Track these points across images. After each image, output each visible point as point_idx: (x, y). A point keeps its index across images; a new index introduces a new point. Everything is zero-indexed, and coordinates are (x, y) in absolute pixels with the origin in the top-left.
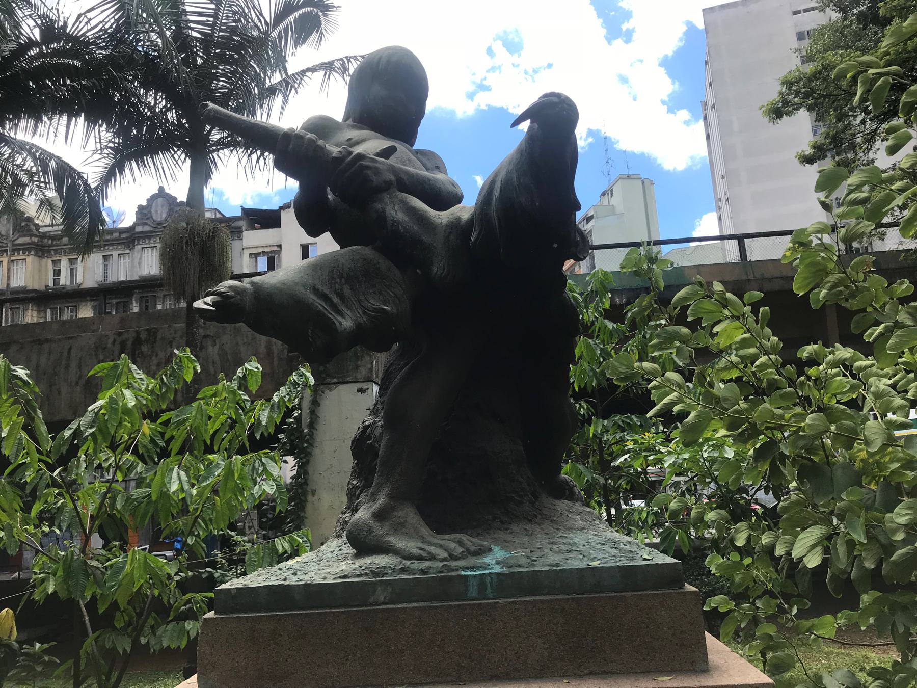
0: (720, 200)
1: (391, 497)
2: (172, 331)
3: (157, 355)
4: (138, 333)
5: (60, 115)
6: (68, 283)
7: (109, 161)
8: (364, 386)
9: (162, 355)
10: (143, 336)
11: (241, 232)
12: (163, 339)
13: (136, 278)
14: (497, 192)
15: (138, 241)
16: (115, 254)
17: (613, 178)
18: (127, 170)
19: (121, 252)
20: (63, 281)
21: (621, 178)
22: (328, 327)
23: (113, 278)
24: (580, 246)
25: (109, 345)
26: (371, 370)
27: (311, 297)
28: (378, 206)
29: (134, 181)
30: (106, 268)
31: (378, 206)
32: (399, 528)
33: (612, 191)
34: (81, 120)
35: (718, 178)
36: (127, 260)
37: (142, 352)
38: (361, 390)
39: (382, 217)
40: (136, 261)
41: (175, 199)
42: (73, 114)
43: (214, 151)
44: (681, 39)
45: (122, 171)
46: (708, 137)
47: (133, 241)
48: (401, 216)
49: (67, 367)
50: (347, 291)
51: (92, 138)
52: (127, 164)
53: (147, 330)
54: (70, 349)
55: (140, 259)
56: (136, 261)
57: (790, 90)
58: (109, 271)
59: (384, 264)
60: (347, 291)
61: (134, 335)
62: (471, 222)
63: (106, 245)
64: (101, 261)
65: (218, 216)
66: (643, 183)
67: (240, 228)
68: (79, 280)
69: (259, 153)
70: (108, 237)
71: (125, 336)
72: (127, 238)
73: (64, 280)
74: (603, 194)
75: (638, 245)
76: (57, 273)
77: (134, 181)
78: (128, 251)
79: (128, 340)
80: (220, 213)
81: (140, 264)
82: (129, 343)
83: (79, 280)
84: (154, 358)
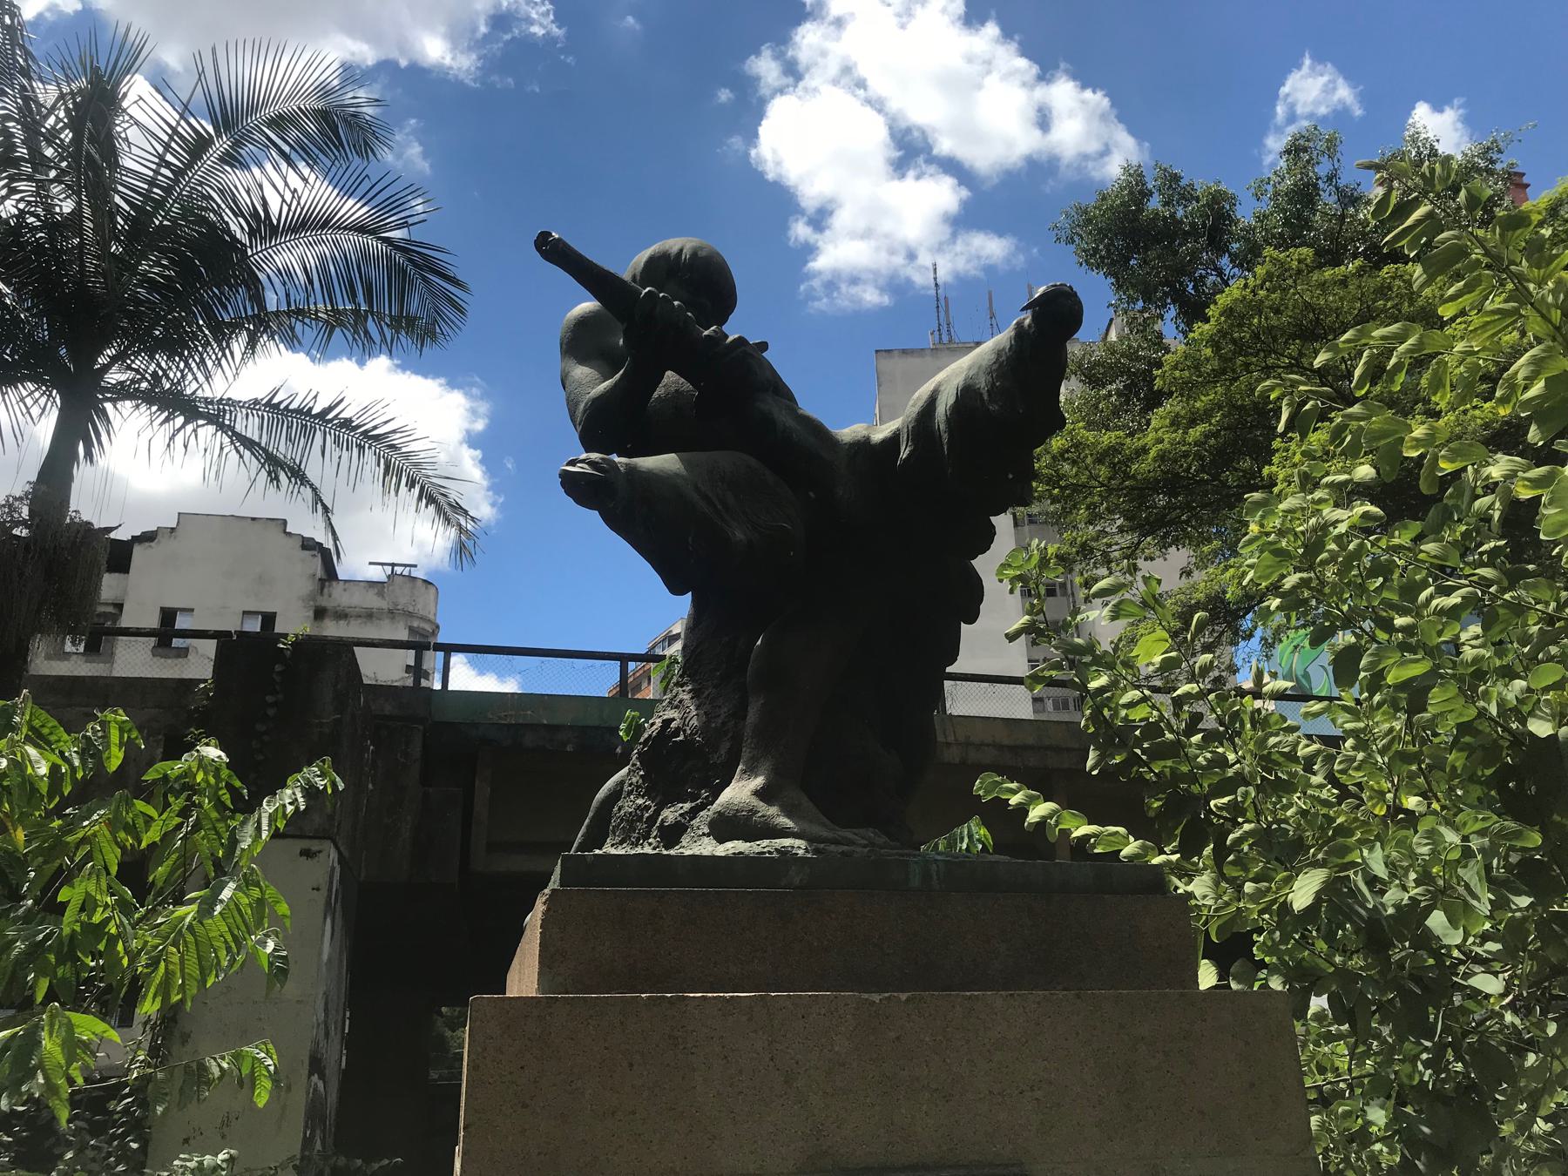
8: (314, 845)
14: (941, 410)
38: (307, 853)
48: (791, 422)
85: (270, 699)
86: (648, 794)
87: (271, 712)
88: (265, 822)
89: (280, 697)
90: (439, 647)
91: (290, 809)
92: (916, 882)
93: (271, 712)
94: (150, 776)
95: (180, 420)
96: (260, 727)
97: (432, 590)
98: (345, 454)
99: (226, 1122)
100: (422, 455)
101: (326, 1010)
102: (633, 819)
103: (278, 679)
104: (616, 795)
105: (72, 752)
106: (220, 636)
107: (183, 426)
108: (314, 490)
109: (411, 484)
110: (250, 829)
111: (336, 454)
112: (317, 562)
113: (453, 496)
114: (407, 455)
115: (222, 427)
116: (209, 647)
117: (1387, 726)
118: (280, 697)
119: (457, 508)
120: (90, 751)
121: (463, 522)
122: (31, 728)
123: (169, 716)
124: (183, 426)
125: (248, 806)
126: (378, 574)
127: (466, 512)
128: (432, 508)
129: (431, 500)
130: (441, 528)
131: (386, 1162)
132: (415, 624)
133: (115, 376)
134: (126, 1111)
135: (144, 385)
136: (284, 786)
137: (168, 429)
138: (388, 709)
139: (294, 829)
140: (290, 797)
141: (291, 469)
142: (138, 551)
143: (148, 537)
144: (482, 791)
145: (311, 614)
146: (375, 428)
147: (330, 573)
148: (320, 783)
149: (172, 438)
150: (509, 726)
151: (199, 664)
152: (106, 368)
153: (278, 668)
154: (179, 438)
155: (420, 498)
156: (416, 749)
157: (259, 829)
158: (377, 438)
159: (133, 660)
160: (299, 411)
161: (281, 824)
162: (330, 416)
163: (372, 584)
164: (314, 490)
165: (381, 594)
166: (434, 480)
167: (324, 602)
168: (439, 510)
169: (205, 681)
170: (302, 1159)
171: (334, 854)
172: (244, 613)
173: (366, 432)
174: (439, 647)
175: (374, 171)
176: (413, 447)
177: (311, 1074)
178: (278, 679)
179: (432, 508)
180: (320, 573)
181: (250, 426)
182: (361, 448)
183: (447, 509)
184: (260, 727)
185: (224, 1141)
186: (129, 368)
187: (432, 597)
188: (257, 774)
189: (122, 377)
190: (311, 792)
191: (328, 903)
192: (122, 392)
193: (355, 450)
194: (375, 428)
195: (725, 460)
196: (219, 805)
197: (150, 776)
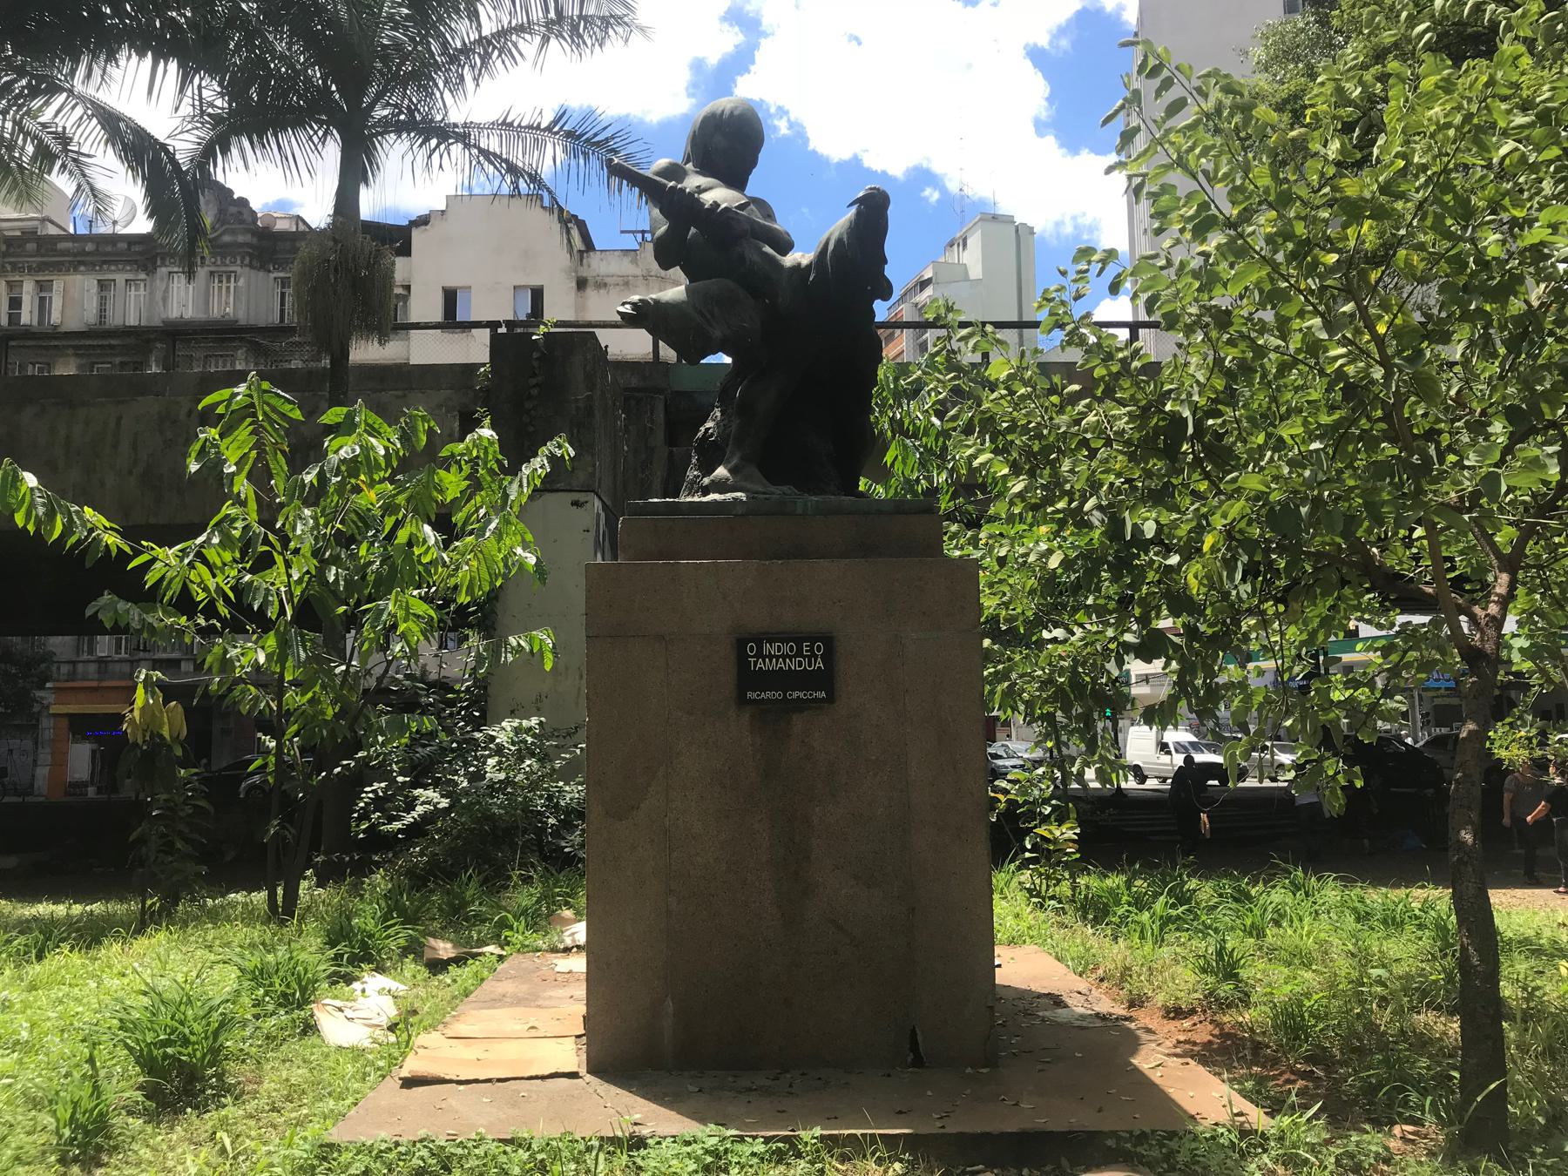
1: (742, 459)
5: (142, 55)
6: (35, 323)
7: (205, 134)
8: (581, 497)
13: (157, 322)
14: (831, 247)
15: (163, 259)
16: (120, 278)
18: (235, 151)
19: (130, 276)
20: (25, 319)
23: (114, 320)
24: (885, 291)
25: (182, 417)
26: (592, 475)
29: (247, 167)
30: (103, 302)
34: (173, 66)
35: (1138, 232)
36: (142, 292)
38: (576, 504)
40: (159, 295)
41: (230, 192)
42: (161, 55)
43: (376, 135)
44: (1061, 31)
45: (225, 151)
47: (153, 260)
48: (756, 258)
49: (115, 446)
51: (187, 100)
52: (234, 139)
54: (120, 419)
55: (166, 290)
56: (159, 295)
58: (109, 307)
62: (809, 266)
63: (105, 262)
64: (95, 289)
65: (302, 227)
68: (55, 317)
70: (109, 249)
72: (140, 253)
73: (27, 316)
76: (15, 303)
77: (247, 167)
78: (143, 276)
80: (305, 222)
81: (165, 300)
83: (55, 317)
85: (533, 381)
86: (699, 469)
87: (535, 392)
92: (799, 511)
93: (535, 392)
94: (444, 453)
95: (434, 142)
96: (528, 405)
99: (539, 699)
100: (639, 156)
102: (693, 482)
103: (536, 364)
105: (394, 438)
106: (493, 325)
107: (438, 146)
108: (550, 192)
110: (515, 486)
115: (467, 146)
116: (484, 335)
120: (405, 438)
122: (367, 424)
123: (460, 396)
124: (438, 146)
125: (514, 470)
133: (380, 112)
134: (468, 688)
135: (402, 117)
136: (535, 455)
137: (424, 151)
138: (634, 382)
139: (549, 485)
140: (538, 466)
141: (530, 175)
142: (417, 235)
143: (423, 221)
145: (574, 284)
146: (596, 135)
148: (558, 453)
149: (430, 157)
151: (475, 349)
152: (371, 106)
153: (535, 355)
154: (436, 156)
156: (660, 416)
157: (521, 486)
158: (598, 144)
159: (428, 349)
160: (530, 127)
161: (538, 482)
164: (550, 192)
165: (634, 262)
167: (584, 272)
169: (484, 365)
171: (597, 503)
173: (588, 140)
175: (311, 925)
178: (536, 364)
181: (492, 143)
182: (585, 154)
185: (538, 712)
186: (388, 104)
188: (517, 450)
189: (385, 112)
190: (552, 459)
191: (597, 542)
192: (389, 126)
194: (596, 135)
196: (491, 472)
197: (444, 453)
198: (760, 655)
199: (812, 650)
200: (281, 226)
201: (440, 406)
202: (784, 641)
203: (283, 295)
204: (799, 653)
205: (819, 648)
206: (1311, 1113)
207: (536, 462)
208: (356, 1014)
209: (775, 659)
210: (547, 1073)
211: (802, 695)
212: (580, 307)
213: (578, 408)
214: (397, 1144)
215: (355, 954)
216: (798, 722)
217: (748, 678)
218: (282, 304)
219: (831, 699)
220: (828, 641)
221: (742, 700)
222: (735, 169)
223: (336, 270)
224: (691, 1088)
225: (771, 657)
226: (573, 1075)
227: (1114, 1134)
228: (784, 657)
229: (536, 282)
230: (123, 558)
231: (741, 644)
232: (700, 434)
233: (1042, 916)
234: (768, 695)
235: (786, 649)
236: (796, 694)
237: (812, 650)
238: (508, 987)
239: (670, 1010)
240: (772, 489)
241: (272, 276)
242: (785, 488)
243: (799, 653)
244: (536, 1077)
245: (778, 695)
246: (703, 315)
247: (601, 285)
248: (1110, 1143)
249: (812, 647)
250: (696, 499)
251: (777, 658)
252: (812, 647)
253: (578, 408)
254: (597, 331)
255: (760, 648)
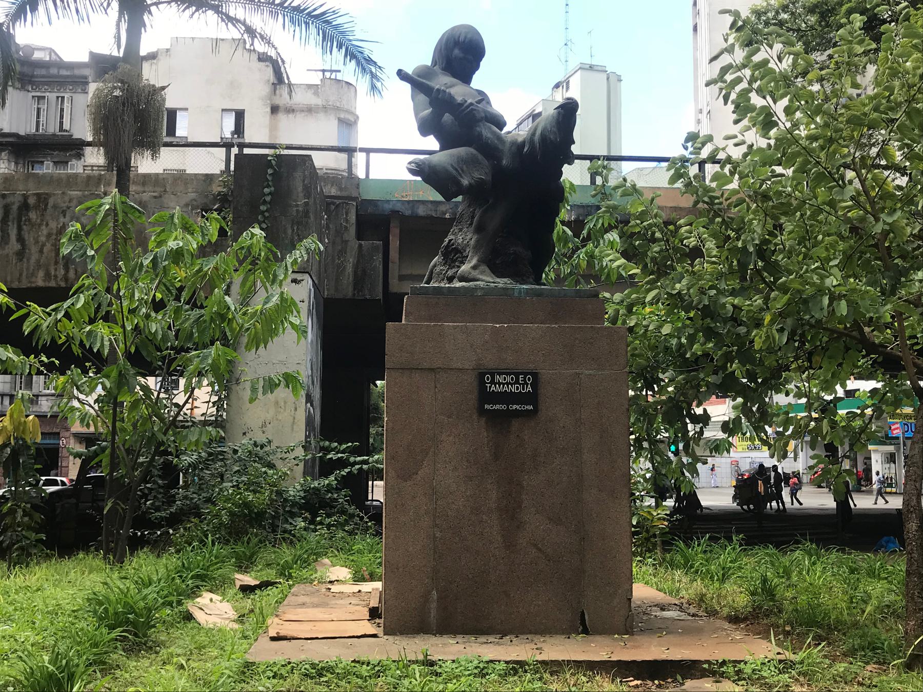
0: (701, 111)
1: (478, 261)
2: (67, 198)
3: (47, 225)
4: (25, 197)
8: (299, 277)
9: (53, 225)
10: (32, 201)
11: (87, 83)
12: (55, 207)
14: (538, 132)
17: (573, 64)
18: (41, 8)
21: (582, 68)
22: (458, 183)
27: (451, 169)
28: (478, 129)
29: (50, 23)
31: (478, 129)
32: (482, 273)
33: (568, 83)
37: (29, 220)
39: (480, 135)
45: (34, 9)
46: (695, 29)
48: (489, 135)
50: (465, 168)
53: (38, 195)
57: (759, 19)
59: (480, 157)
60: (465, 168)
61: (21, 199)
62: (524, 143)
65: (54, 57)
66: (608, 79)
67: (86, 77)
69: (194, 8)
71: (8, 200)
74: (557, 86)
75: (598, 158)
79: (13, 204)
80: (56, 54)
82: (15, 207)
84: (44, 227)
85: (266, 190)
88: (289, 266)
89: (273, 189)
90: (362, 150)
91: (300, 260)
93: (268, 198)
96: (263, 208)
97: (352, 90)
98: (297, 29)
100: (346, 26)
101: (312, 369)
102: (439, 274)
104: (435, 266)
109: (340, 47)
111: (292, 29)
112: (269, 73)
113: (367, 53)
114: (336, 27)
117: (895, 217)
118: (273, 189)
119: (370, 61)
121: (374, 70)
126: (316, 79)
127: (375, 63)
128: (354, 62)
129: (353, 56)
130: (360, 75)
131: (350, 444)
132: (342, 116)
138: (334, 191)
144: (395, 243)
145: (269, 110)
146: (315, 10)
147: (279, 78)
148: (313, 247)
150: (409, 202)
153: (270, 171)
155: (346, 56)
156: (353, 217)
158: (316, 17)
162: (286, 5)
163: (309, 86)
165: (316, 94)
166: (354, 43)
167: (278, 101)
168: (358, 63)
170: (306, 442)
171: (310, 282)
172: (223, 110)
173: (309, 14)
174: (362, 150)
176: (339, 21)
177: (306, 403)
178: (269, 178)
179: (354, 62)
180: (272, 79)
182: (307, 24)
183: (363, 60)
184: (263, 208)
187: (353, 94)
190: (308, 250)
191: (309, 310)
193: (303, 26)
194: (315, 10)
195: (462, 151)
198: (493, 382)
199: (525, 380)
200: (37, 55)
201: (187, 205)
202: (507, 374)
203: (39, 109)
204: (517, 382)
205: (529, 379)
206: (820, 647)
207: (297, 253)
208: (214, 610)
209: (503, 385)
210: (359, 634)
211: (518, 407)
212: (273, 128)
213: (297, 211)
214: (289, 663)
215: (205, 580)
216: (515, 424)
217: (485, 396)
218: (38, 117)
219: (535, 411)
220: (535, 375)
221: (482, 412)
222: (465, 75)
223: (124, 104)
224: (451, 641)
225: (500, 384)
226: (375, 636)
227: (708, 662)
228: (508, 384)
229: (239, 107)
230: (10, 312)
231: (481, 376)
232: (445, 244)
233: (644, 568)
234: (497, 407)
235: (509, 379)
236: (514, 407)
237: (525, 380)
238: (302, 599)
239: (435, 597)
240: (498, 280)
241: (31, 94)
242: (506, 280)
243: (517, 382)
244: (353, 637)
245: (504, 407)
246: (456, 170)
247: (290, 110)
248: (706, 666)
249: (525, 378)
250: (442, 285)
251: (504, 384)
252: (525, 378)
253: (297, 211)
254: (314, 154)
255: (493, 378)
